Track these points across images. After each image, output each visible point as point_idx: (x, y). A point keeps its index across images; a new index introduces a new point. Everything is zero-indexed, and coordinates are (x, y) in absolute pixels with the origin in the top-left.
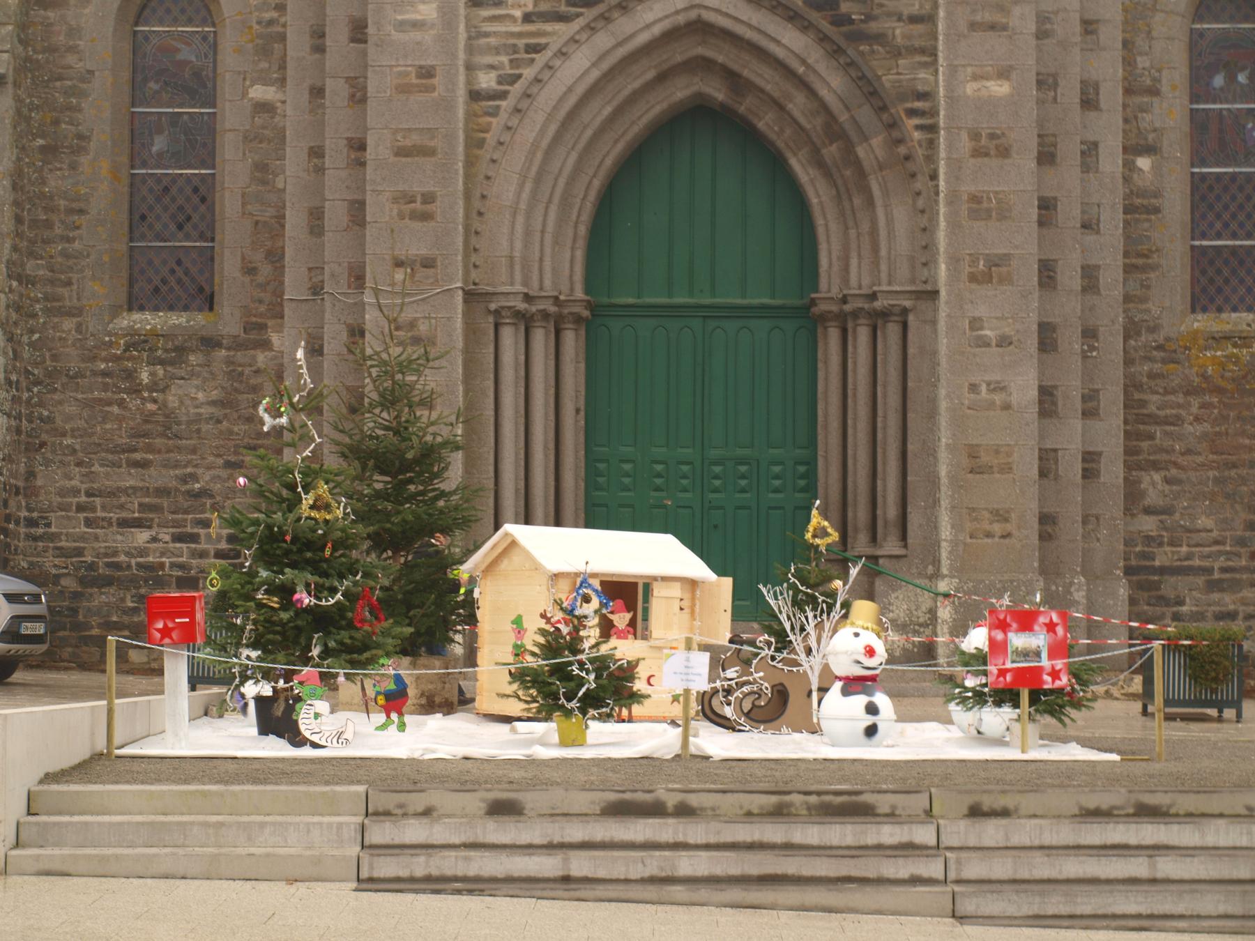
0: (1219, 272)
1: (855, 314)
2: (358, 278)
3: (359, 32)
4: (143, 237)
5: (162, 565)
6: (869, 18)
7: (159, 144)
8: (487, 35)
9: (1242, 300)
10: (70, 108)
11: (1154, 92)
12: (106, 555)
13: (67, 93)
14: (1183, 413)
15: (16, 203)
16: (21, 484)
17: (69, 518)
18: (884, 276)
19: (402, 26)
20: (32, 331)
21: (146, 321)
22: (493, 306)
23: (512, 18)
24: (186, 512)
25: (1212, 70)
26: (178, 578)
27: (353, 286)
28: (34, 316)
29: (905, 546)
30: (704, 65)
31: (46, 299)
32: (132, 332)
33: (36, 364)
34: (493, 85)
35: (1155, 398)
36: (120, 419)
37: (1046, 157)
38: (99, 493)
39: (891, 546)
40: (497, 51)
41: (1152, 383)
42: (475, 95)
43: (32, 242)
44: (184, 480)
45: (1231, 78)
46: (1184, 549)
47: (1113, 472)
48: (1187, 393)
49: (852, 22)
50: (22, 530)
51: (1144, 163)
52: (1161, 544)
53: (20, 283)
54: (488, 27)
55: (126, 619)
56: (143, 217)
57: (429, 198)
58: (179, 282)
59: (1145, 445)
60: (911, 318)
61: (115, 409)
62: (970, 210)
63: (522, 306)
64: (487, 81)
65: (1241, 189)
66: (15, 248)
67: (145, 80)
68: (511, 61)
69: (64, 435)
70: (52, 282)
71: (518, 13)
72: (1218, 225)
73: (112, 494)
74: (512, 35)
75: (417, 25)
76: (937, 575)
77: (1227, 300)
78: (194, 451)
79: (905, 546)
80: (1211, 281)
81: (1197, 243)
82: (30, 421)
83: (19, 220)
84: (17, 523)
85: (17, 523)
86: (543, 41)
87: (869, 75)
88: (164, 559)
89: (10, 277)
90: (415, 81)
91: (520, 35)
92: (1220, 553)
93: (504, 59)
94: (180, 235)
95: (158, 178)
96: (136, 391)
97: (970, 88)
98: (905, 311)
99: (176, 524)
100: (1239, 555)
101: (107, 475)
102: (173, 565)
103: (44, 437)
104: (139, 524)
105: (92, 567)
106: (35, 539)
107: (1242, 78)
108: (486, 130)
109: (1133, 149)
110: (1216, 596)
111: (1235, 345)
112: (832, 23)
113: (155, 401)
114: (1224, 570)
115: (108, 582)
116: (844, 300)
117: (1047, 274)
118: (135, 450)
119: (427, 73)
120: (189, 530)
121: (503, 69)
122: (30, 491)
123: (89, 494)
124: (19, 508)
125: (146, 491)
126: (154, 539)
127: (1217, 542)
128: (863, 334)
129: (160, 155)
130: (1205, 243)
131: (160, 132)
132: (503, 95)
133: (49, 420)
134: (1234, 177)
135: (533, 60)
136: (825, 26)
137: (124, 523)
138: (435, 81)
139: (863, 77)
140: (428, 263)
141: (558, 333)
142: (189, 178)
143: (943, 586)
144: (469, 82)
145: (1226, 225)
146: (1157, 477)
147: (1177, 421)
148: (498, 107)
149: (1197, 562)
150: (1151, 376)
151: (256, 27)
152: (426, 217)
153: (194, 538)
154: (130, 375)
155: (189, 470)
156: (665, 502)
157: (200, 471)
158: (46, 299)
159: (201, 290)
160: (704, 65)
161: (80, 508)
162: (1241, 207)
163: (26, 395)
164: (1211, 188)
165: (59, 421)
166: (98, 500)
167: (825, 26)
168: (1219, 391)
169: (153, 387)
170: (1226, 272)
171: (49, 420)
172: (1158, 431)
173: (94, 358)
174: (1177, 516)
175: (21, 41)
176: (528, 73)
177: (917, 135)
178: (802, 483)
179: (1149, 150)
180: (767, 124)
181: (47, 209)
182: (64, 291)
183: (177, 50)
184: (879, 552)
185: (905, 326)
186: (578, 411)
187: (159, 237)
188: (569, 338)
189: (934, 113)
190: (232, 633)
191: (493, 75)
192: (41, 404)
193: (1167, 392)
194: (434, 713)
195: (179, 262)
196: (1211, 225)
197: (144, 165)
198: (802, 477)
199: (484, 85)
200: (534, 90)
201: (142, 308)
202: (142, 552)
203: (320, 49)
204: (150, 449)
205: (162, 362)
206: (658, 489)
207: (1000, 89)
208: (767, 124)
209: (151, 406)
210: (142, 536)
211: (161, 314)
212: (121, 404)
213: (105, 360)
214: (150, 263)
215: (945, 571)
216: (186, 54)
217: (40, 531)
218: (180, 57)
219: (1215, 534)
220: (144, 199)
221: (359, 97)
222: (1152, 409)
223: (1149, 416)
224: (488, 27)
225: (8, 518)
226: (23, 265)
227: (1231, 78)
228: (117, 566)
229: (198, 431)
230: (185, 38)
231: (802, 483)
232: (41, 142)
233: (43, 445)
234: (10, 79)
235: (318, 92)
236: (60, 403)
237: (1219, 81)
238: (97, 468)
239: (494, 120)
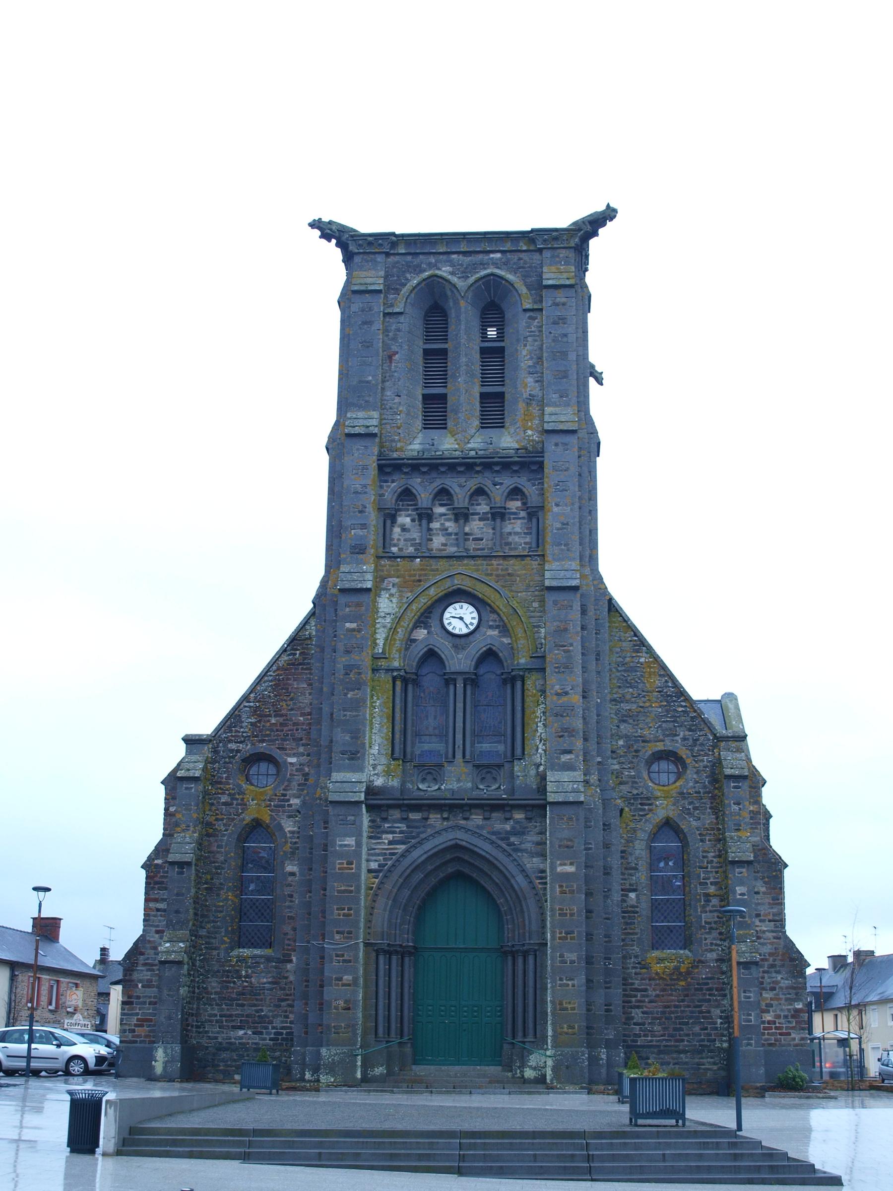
0: (663, 935)
1: (517, 951)
4: (245, 921)
5: (248, 1043)
6: (521, 843)
7: (252, 887)
9: (672, 945)
10: (217, 873)
11: (636, 869)
12: (227, 1039)
13: (216, 868)
14: (649, 987)
15: (195, 908)
16: (194, 1012)
17: (213, 1025)
18: (527, 938)
19: (341, 846)
20: (200, 955)
21: (246, 952)
22: (375, 948)
24: (258, 1023)
25: (659, 861)
26: (254, 1048)
27: (97, 969)
28: (201, 950)
29: (536, 1038)
30: (458, 859)
31: (206, 943)
32: (238, 956)
33: (201, 968)
34: (377, 867)
35: (637, 982)
36: (233, 988)
38: (224, 1016)
39: (530, 1038)
40: (378, 855)
41: (636, 976)
43: (201, 922)
44: (257, 1011)
45: (667, 864)
48: (650, 980)
49: (515, 845)
50: (194, 1029)
51: (632, 895)
52: (640, 1037)
53: (196, 937)
55: (234, 1064)
56: (245, 914)
58: (258, 937)
59: (634, 999)
60: (538, 953)
61: (232, 985)
62: (559, 914)
63: (387, 948)
65: (671, 904)
66: (194, 925)
67: (247, 863)
69: (211, 994)
70: (208, 937)
72: (662, 918)
73: (231, 1016)
76: (547, 1049)
77: (666, 945)
78: (261, 1001)
79: (536, 1038)
80: (660, 938)
82: (198, 989)
83: (196, 914)
84: (192, 1026)
85: (192, 1026)
86: (396, 851)
87: (521, 864)
89: (192, 936)
92: (664, 1040)
94: (259, 920)
95: (251, 900)
96: (240, 977)
97: (559, 869)
98: (535, 951)
99: (255, 1028)
100: (670, 1040)
101: (228, 1009)
102: (253, 1043)
103: (204, 995)
104: (240, 1028)
105: (220, 1043)
106: (199, 1033)
107: (671, 863)
110: (662, 1056)
111: (668, 962)
112: (508, 845)
113: (247, 982)
114: (665, 1046)
115: (226, 1049)
116: (513, 946)
118: (239, 1000)
120: (259, 1030)
122: (198, 1015)
123: (221, 1016)
124: (193, 1021)
125: (242, 1016)
126: (246, 1034)
127: (662, 1036)
128: (520, 960)
129: (252, 891)
131: (252, 883)
132: (380, 871)
133: (206, 988)
134: (668, 900)
136: (504, 846)
137: (235, 1028)
138: (354, 866)
139: (519, 865)
141: (390, 959)
142: (263, 900)
143: (548, 1053)
144: (367, 866)
145: (665, 918)
147: (645, 990)
149: (654, 1043)
150: (636, 974)
153: (261, 1033)
154: (238, 971)
155: (260, 1008)
157: (264, 1008)
158: (206, 943)
159: (267, 941)
160: (458, 859)
161: (217, 1021)
162: (671, 911)
163: (197, 979)
164: (659, 904)
165: (210, 989)
166: (224, 1019)
167: (504, 846)
168: (664, 979)
169: (247, 976)
170: (666, 935)
171: (206, 988)
172: (639, 994)
173: (224, 966)
174: (646, 1026)
175: (198, 849)
177: (540, 886)
178: (499, 1014)
181: (207, 911)
182: (213, 941)
183: (260, 852)
184: (525, 1040)
185: (536, 955)
187: (251, 921)
188: (407, 960)
189: (546, 878)
190: (329, 1062)
191: (377, 864)
192: (203, 982)
193: (642, 979)
195: (259, 931)
196: (659, 918)
197: (246, 894)
198: (499, 1012)
200: (392, 869)
201: (244, 947)
202: (241, 1038)
204: (245, 999)
205: (249, 967)
206: (442, 1016)
209: (246, 984)
210: (241, 1032)
212: (234, 982)
213: (227, 966)
214: (247, 930)
215: (550, 1047)
216: (263, 854)
217: (201, 1030)
218: (261, 855)
219: (662, 1032)
220: (245, 907)
222: (636, 986)
223: (636, 989)
225: (188, 1025)
226: (197, 931)
227: (667, 864)
228: (231, 1043)
229: (264, 993)
230: (263, 848)
231: (499, 1014)
232: (206, 886)
233: (203, 998)
234: (194, 863)
236: (210, 982)
237: (662, 864)
238: (224, 1006)
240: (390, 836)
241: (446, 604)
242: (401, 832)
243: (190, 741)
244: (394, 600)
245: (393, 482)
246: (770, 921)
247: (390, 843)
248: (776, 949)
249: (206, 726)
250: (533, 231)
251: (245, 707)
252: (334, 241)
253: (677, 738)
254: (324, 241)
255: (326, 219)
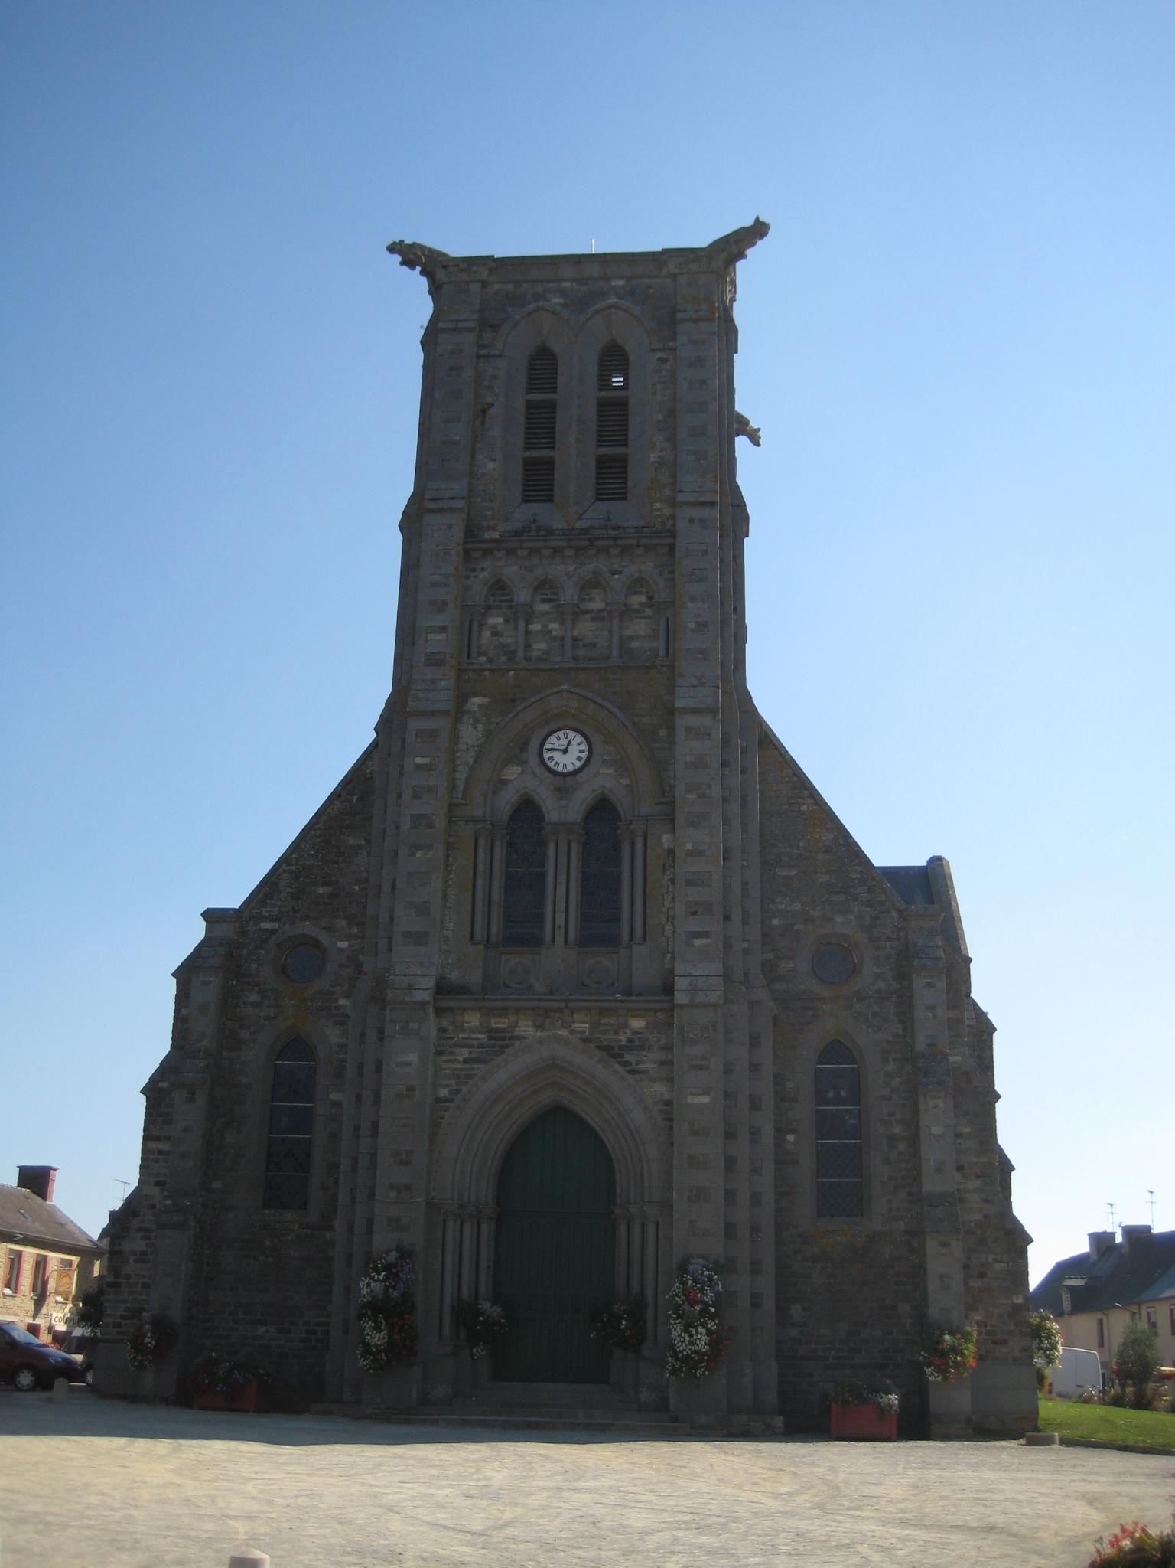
2: (372, 1194)
3: (379, 1067)
8: (444, 1069)
23: (458, 1061)
37: (730, 1135)
42: (438, 1100)
46: (814, 1346)
47: (769, 1304)
51: (790, 1138)
54: (444, 1065)
57: (408, 1153)
64: (443, 1093)
68: (456, 1083)
71: (461, 1058)
74: (457, 1069)
75: (407, 1064)
81: (820, 1180)
88: (272, 1342)
90: (405, 1092)
91: (461, 1069)
93: (453, 1082)
108: (443, 1118)
109: (780, 1132)
117: (730, 1196)
119: (411, 1089)
121: (452, 1086)
130: (824, 1180)
132: (451, 1100)
135: (467, 1083)
140: (408, 1187)
146: (798, 1306)
148: (448, 1106)
151: (335, 1063)
152: (407, 1163)
156: (710, 1308)
176: (464, 1089)
179: (793, 1131)
180: (40, 1297)
186: (488, 1267)
194: (53, 1384)
199: (442, 1095)
203: (361, 1075)
207: (705, 1099)
208: (40, 1297)
210: (261, 1330)
211: (279, 1210)
221: (377, 1101)
224: (444, 1065)
235: (359, 1097)
237: (831, 1094)
239: (447, 1113)
240: (465, 1052)
241: (545, 731)
242: (481, 1046)
243: (212, 916)
244: (480, 727)
245: (483, 570)
246: (977, 1176)
247: (465, 1061)
248: (986, 1216)
249: (233, 897)
250: (665, 252)
251: (284, 871)
252: (418, 269)
253: (851, 917)
254: (405, 268)
255: (408, 241)
